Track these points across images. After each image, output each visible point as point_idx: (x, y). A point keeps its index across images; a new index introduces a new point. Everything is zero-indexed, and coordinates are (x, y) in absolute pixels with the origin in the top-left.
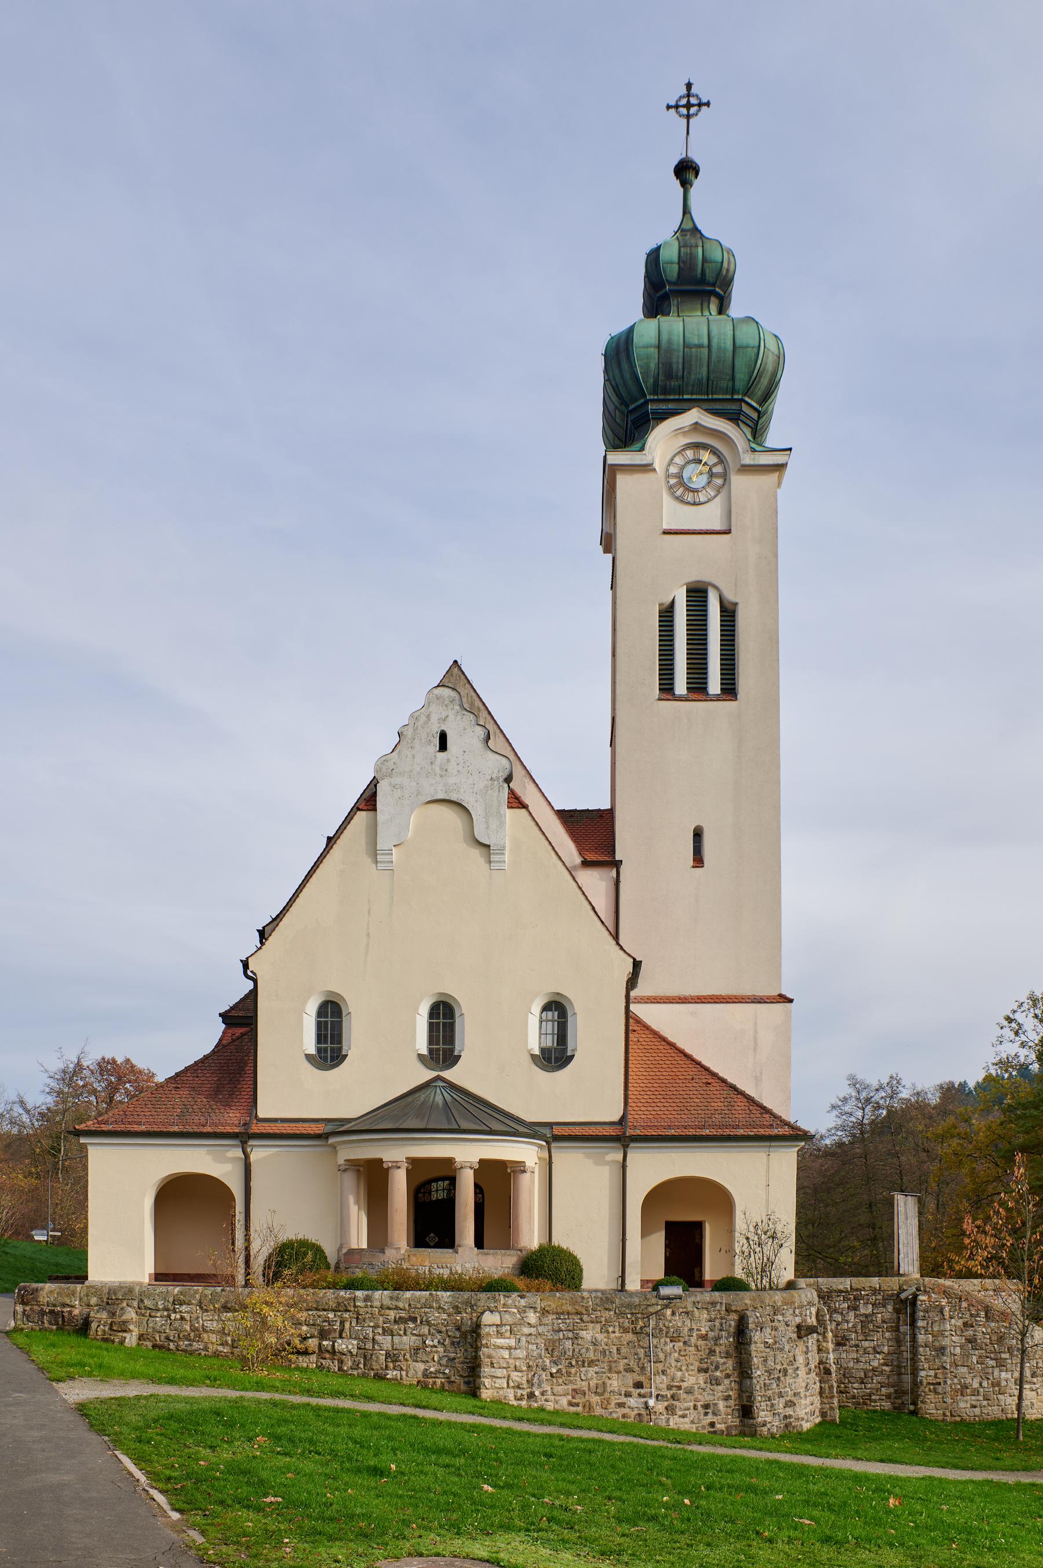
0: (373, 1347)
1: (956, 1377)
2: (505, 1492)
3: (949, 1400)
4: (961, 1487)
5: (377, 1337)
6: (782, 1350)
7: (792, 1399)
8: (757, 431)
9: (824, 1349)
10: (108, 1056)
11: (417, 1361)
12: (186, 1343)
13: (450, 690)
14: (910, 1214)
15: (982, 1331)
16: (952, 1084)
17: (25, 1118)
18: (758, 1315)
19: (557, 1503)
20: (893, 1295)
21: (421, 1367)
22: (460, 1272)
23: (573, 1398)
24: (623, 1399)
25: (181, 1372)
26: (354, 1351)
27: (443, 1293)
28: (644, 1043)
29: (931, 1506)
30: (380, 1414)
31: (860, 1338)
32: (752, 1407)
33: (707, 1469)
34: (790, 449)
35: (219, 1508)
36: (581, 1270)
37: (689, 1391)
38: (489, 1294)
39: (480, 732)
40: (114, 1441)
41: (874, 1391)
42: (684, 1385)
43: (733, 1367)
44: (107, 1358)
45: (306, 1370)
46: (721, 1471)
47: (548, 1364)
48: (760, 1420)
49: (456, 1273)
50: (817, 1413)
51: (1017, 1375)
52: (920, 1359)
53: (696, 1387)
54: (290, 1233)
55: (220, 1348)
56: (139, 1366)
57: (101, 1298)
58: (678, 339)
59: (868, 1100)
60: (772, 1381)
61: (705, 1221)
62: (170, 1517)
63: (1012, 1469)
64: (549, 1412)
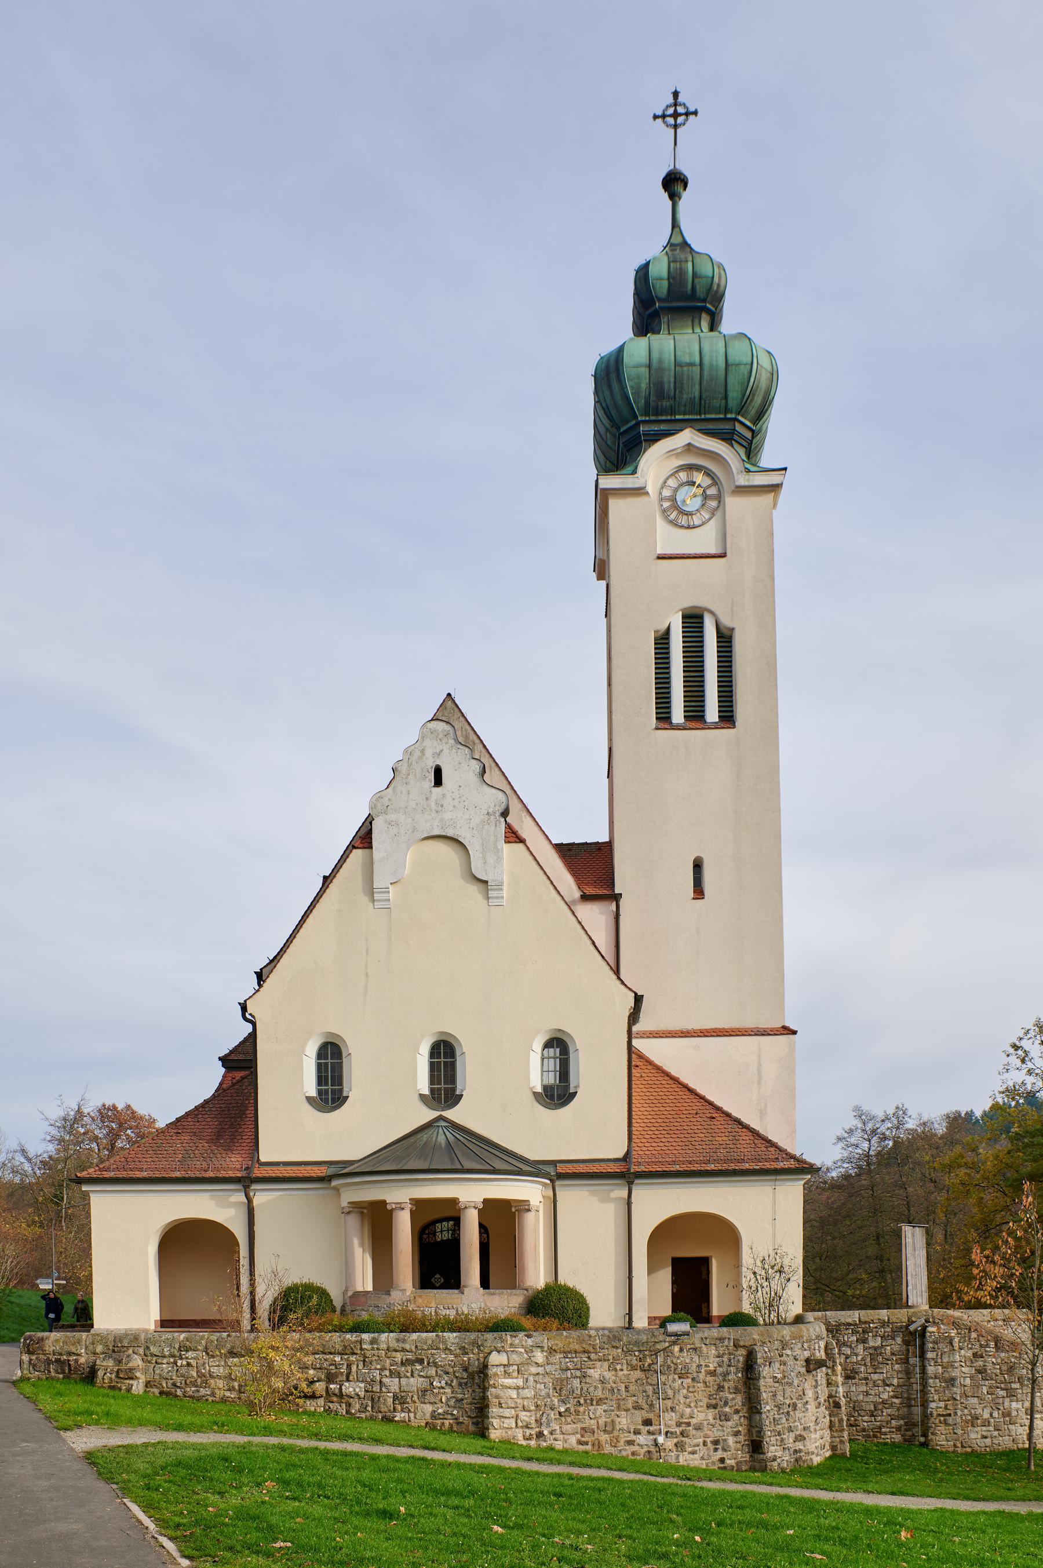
0: (381, 1389)
1: (966, 1408)
2: (515, 1532)
3: (959, 1432)
4: (973, 1518)
5: (385, 1380)
6: (791, 1384)
7: (802, 1433)
8: (751, 450)
9: (833, 1382)
10: (109, 1103)
11: (425, 1403)
12: (193, 1389)
13: (444, 724)
14: (918, 1246)
15: (992, 1361)
16: (959, 1113)
17: (27, 1167)
18: (767, 1350)
19: (568, 1542)
20: (901, 1327)
21: (429, 1408)
22: (466, 1312)
23: (582, 1436)
24: (632, 1437)
25: (189, 1419)
26: (362, 1394)
27: (450, 1334)
28: (647, 1079)
29: (943, 1538)
30: (388, 1457)
31: (869, 1371)
32: (762, 1442)
33: (718, 1505)
34: (785, 469)
35: (228, 1554)
36: (588, 1309)
37: (698, 1428)
38: (496, 1334)
39: (476, 766)
40: (122, 1489)
41: (884, 1424)
42: (693, 1421)
43: (743, 1402)
44: (114, 1405)
45: (313, 1414)
46: (731, 1507)
47: (556, 1403)
48: (770, 1454)
49: (463, 1313)
50: (827, 1447)
51: (1027, 1404)
52: (930, 1391)
53: (705, 1423)
54: (295, 1277)
55: (228, 1394)
56: (146, 1413)
57: (107, 1346)
58: (669, 358)
59: (874, 1132)
60: (782, 1416)
61: (711, 1257)
62: (179, 1564)
63: (1023, 1499)
64: (559, 1451)
